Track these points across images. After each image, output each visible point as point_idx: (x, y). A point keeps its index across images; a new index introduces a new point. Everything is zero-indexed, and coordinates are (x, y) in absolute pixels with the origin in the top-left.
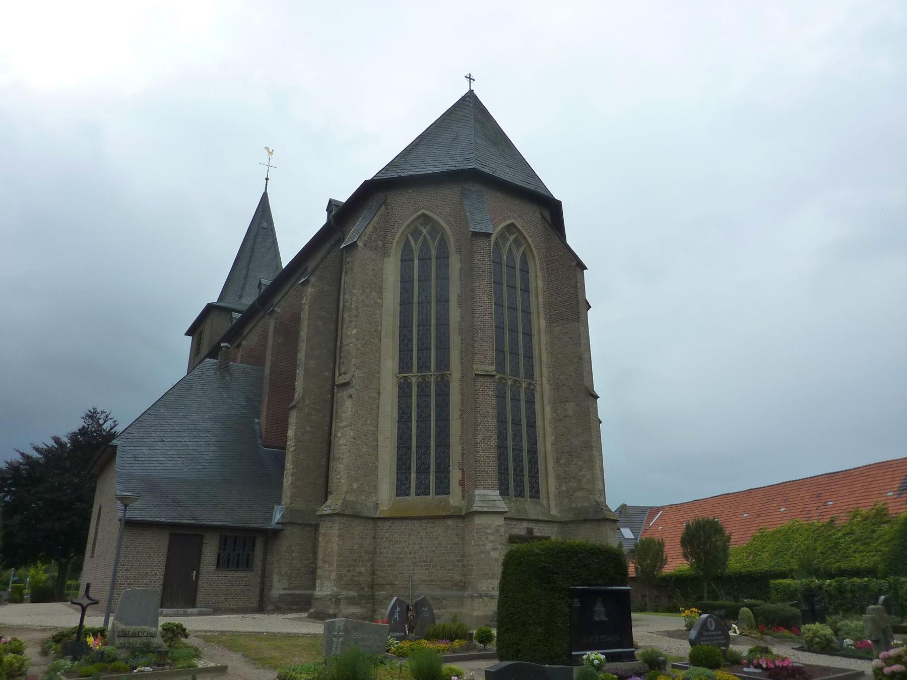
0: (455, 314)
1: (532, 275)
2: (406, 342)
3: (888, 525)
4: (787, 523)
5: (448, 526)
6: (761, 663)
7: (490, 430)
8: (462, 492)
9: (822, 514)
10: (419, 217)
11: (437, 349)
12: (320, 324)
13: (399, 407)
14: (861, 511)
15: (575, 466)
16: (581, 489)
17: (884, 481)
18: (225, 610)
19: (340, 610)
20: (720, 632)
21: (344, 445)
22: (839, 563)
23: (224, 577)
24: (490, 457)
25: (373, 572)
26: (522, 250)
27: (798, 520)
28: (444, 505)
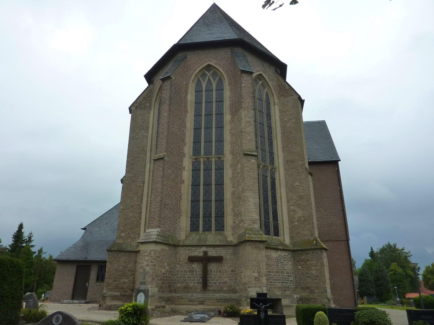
7: (158, 192)
19: (105, 303)
23: (100, 285)
24: (157, 208)
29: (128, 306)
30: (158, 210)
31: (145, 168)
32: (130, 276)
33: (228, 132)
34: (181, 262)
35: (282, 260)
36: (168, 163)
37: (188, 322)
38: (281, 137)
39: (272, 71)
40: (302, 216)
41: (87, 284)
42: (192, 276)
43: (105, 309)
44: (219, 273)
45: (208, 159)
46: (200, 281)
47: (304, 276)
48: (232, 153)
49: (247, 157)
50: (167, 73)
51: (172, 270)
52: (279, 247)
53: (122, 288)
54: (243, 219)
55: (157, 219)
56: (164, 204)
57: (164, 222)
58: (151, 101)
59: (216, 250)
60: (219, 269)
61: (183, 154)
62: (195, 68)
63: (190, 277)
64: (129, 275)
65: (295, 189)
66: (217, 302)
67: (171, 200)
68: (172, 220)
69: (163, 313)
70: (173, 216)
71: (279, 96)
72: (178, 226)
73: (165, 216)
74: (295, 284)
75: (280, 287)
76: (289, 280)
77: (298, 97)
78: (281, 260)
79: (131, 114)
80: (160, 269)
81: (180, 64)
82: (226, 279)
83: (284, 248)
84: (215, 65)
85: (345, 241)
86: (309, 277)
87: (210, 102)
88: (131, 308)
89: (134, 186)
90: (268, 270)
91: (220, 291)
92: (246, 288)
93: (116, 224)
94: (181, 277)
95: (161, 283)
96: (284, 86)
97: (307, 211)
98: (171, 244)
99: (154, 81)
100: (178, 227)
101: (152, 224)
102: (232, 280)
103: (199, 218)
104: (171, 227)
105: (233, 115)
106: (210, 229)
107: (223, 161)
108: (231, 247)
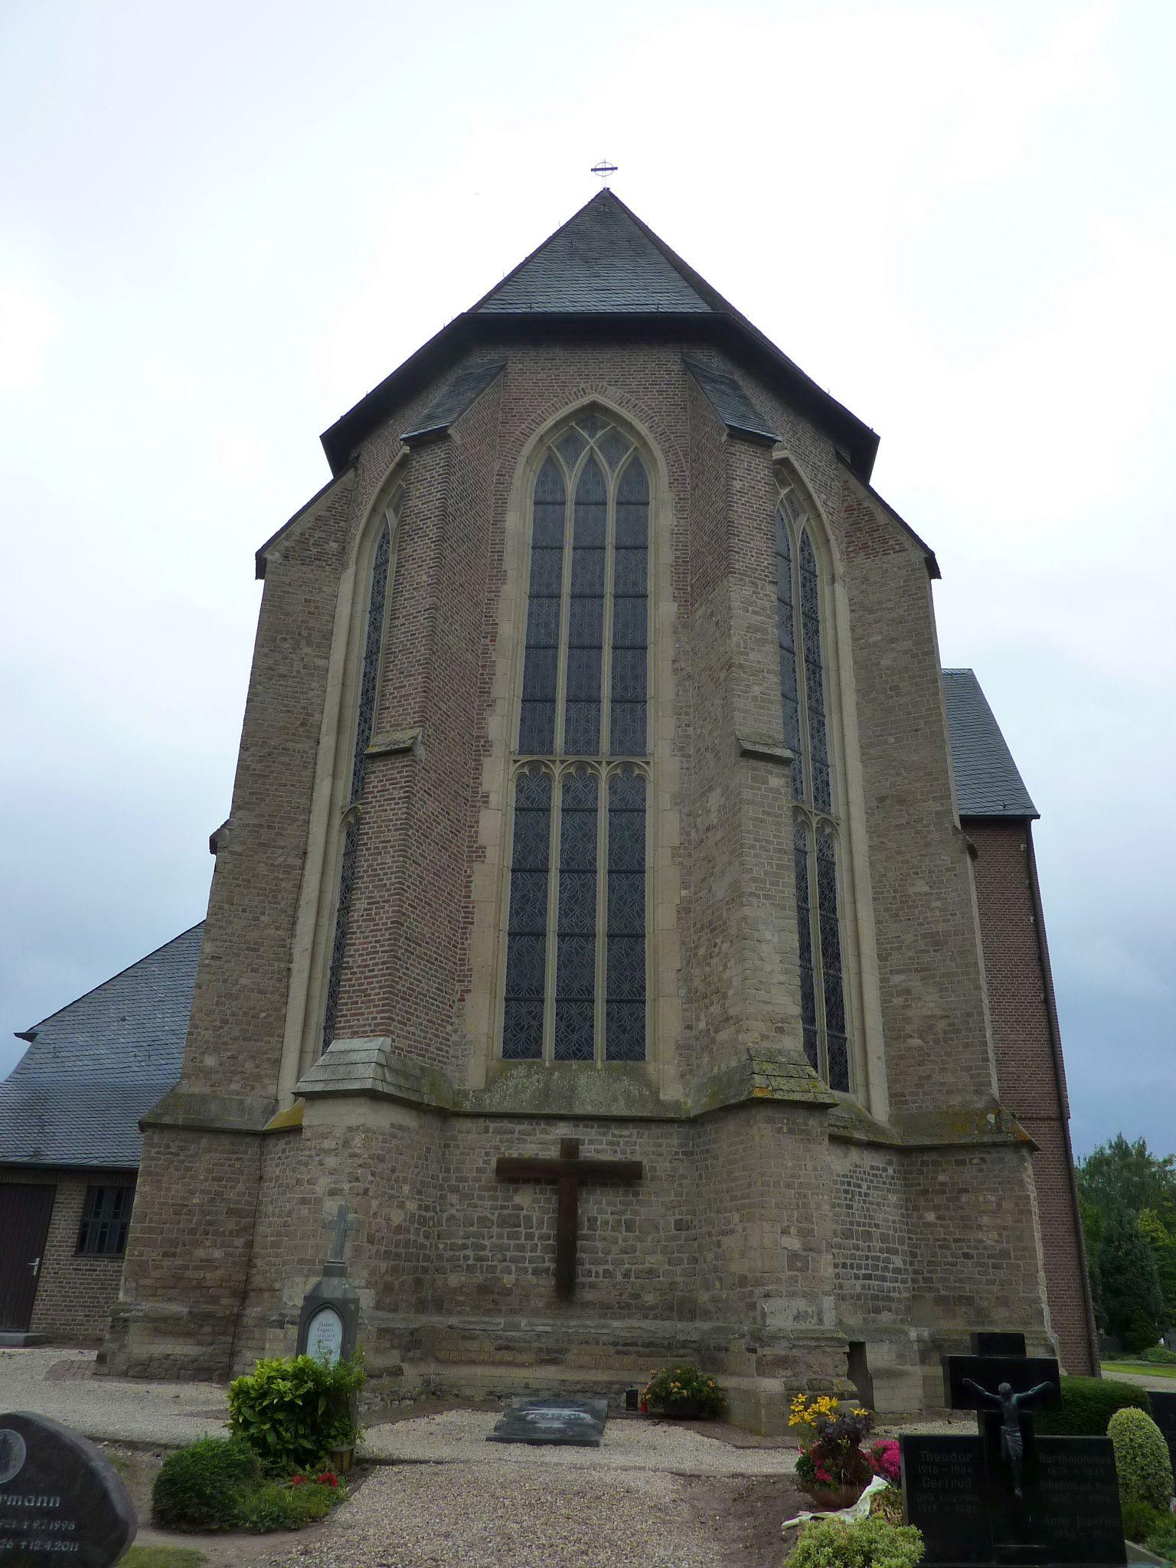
18: (83, 1340)
19: (123, 1346)
20: (55, 1502)
24: (377, 952)
29: (273, 1374)
30: (384, 963)
31: (311, 795)
32: (235, 1233)
33: (666, 667)
34: (466, 1184)
35: (865, 1185)
36: (426, 770)
37: (519, 1445)
38: (857, 703)
39: (823, 454)
40: (939, 1012)
41: (37, 1263)
42: (512, 1242)
43: (124, 1375)
44: (624, 1233)
45: (582, 766)
46: (547, 1264)
47: (948, 1253)
48: (681, 749)
49: (753, 763)
50: (430, 417)
51: (428, 1215)
52: (857, 1135)
53: (200, 1286)
54: (732, 1012)
55: (379, 1000)
56: (406, 938)
57: (406, 1012)
58: (346, 532)
59: (614, 1135)
60: (623, 1218)
61: (482, 743)
62: (540, 412)
63: (502, 1248)
64: (231, 1232)
65: (909, 907)
66: (618, 1353)
67: (433, 924)
68: (433, 1004)
69: (391, 1401)
70: (438, 989)
71: (850, 549)
72: (455, 1031)
73: (408, 988)
74: (909, 1284)
75: (859, 1297)
76: (891, 1266)
77: (926, 558)
78: (861, 1188)
79: (262, 582)
80: (386, 1210)
81: (485, 388)
82: (653, 1260)
83: (873, 1138)
84: (617, 407)
85: (1051, 1119)
86: (966, 1256)
87: (594, 548)
88: (289, 1384)
89: (262, 865)
90: (862, 1228)
91: (628, 1306)
92: (749, 1300)
93: (158, 1020)
94: (465, 1247)
95: (387, 1271)
96: (871, 514)
97: (959, 996)
98: (428, 1105)
99: (362, 459)
100: (454, 1038)
101: (354, 1020)
102: (680, 1261)
103: (542, 1001)
104: (429, 1036)
105: (685, 601)
106: (585, 1049)
107: (642, 779)
108: (676, 1126)
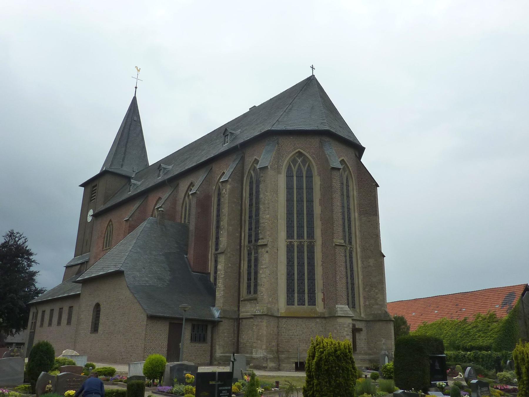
0: (317, 210)
1: (351, 188)
2: (290, 222)
3: (496, 323)
4: (439, 320)
5: (317, 322)
6: (498, 387)
8: (324, 305)
9: (460, 315)
10: (297, 153)
11: (307, 227)
12: (234, 206)
13: (287, 257)
14: (481, 315)
15: (373, 292)
16: (377, 304)
17: (494, 299)
19: (268, 365)
21: (264, 278)
22: (471, 343)
25: (278, 345)
26: (346, 173)
27: (446, 318)
28: (314, 311)
